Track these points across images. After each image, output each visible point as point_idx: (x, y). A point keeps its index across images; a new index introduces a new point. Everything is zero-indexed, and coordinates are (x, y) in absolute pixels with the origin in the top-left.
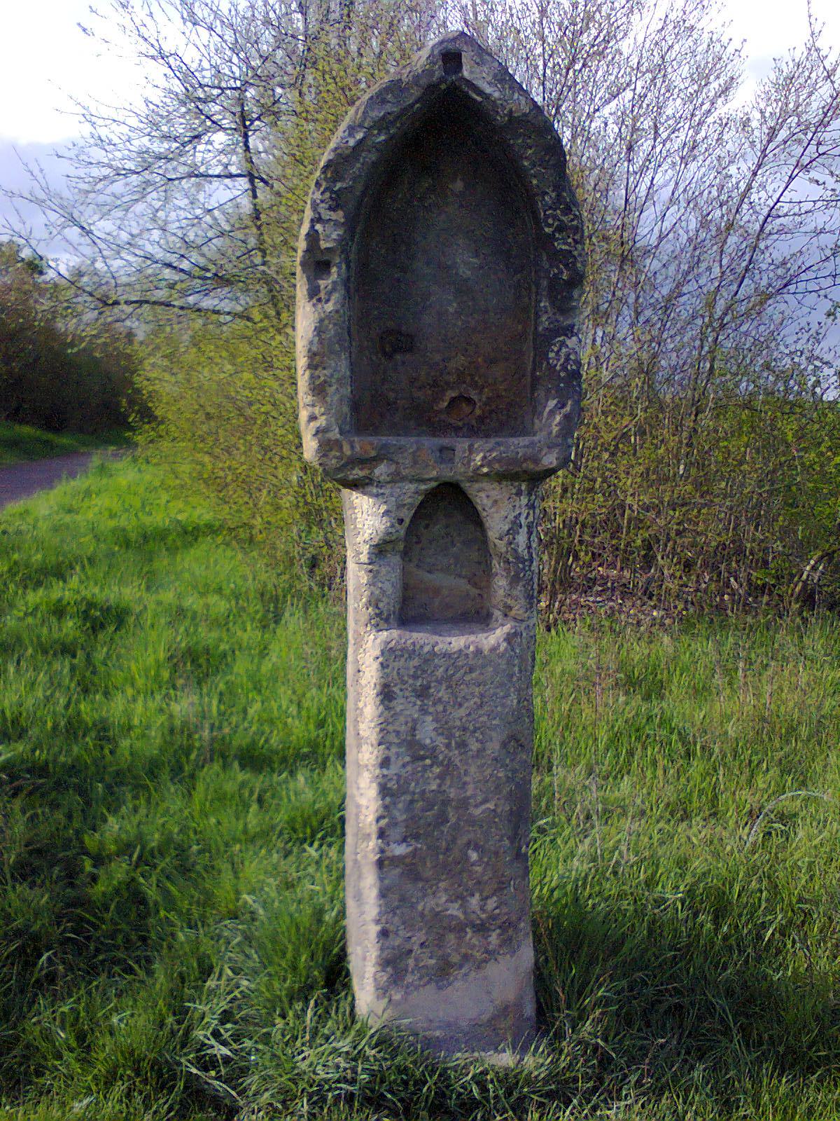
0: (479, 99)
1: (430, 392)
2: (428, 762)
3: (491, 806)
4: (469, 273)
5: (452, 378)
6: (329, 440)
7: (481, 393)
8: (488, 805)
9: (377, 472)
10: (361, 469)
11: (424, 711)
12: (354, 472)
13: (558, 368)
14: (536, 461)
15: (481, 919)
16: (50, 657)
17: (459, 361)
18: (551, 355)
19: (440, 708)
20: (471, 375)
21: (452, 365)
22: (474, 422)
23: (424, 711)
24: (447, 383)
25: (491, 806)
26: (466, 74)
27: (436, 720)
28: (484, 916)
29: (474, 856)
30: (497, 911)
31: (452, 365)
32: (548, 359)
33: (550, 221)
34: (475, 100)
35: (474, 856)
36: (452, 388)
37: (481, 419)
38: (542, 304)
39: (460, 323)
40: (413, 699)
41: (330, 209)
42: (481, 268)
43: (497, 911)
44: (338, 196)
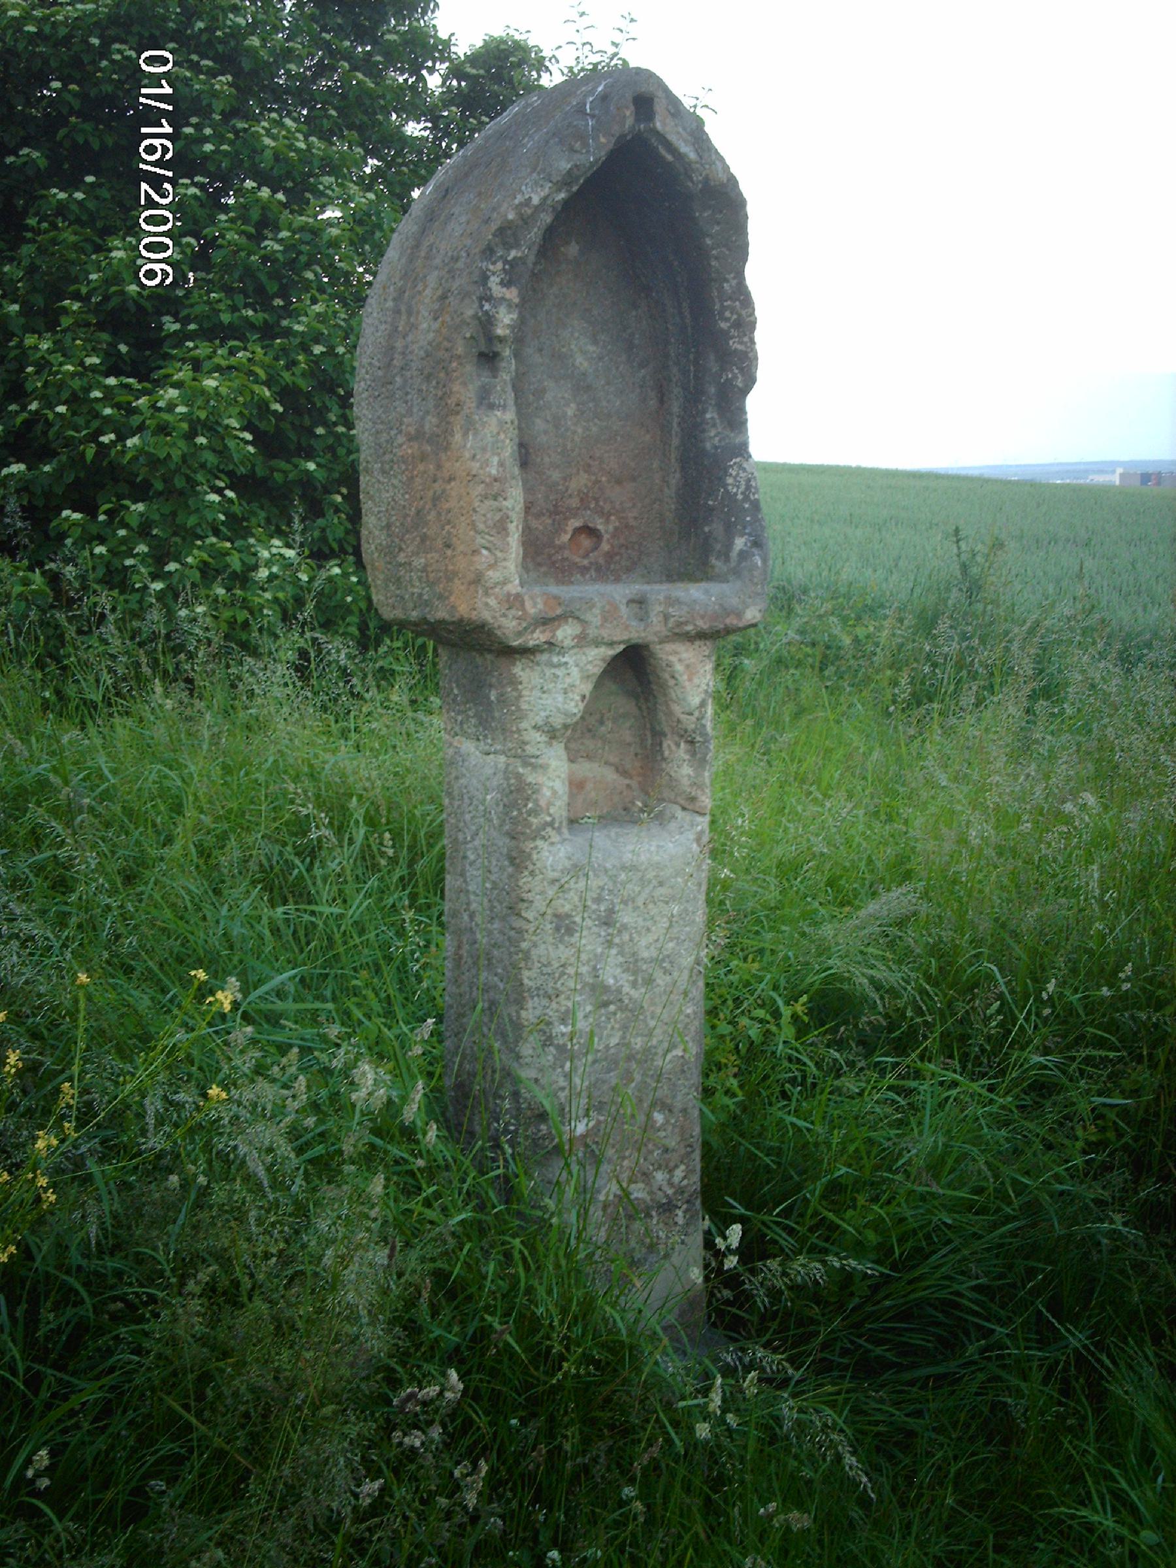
0: (669, 158)
1: (549, 521)
2: (612, 1008)
3: (678, 1052)
4: (586, 364)
5: (574, 502)
6: (509, 594)
7: (607, 521)
8: (674, 1053)
9: (560, 634)
10: (543, 632)
11: (609, 944)
12: (535, 635)
13: (740, 497)
14: (739, 615)
15: (667, 1196)
16: (549, 911)
17: (580, 481)
18: (730, 481)
19: (626, 937)
20: (596, 500)
21: (573, 485)
22: (601, 561)
23: (609, 944)
24: (569, 509)
25: (678, 1052)
26: (658, 125)
27: (621, 953)
28: (670, 1192)
29: (659, 1118)
30: (685, 1182)
31: (573, 485)
32: (725, 486)
33: (727, 314)
34: (663, 157)
35: (659, 1118)
36: (575, 516)
37: (610, 556)
38: (708, 416)
39: (580, 431)
40: (595, 929)
41: (502, 283)
42: (600, 358)
43: (685, 1182)
44: (512, 266)
